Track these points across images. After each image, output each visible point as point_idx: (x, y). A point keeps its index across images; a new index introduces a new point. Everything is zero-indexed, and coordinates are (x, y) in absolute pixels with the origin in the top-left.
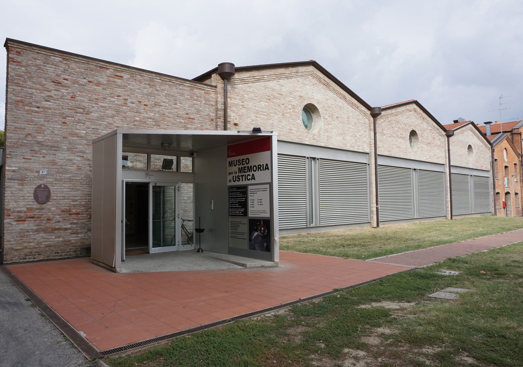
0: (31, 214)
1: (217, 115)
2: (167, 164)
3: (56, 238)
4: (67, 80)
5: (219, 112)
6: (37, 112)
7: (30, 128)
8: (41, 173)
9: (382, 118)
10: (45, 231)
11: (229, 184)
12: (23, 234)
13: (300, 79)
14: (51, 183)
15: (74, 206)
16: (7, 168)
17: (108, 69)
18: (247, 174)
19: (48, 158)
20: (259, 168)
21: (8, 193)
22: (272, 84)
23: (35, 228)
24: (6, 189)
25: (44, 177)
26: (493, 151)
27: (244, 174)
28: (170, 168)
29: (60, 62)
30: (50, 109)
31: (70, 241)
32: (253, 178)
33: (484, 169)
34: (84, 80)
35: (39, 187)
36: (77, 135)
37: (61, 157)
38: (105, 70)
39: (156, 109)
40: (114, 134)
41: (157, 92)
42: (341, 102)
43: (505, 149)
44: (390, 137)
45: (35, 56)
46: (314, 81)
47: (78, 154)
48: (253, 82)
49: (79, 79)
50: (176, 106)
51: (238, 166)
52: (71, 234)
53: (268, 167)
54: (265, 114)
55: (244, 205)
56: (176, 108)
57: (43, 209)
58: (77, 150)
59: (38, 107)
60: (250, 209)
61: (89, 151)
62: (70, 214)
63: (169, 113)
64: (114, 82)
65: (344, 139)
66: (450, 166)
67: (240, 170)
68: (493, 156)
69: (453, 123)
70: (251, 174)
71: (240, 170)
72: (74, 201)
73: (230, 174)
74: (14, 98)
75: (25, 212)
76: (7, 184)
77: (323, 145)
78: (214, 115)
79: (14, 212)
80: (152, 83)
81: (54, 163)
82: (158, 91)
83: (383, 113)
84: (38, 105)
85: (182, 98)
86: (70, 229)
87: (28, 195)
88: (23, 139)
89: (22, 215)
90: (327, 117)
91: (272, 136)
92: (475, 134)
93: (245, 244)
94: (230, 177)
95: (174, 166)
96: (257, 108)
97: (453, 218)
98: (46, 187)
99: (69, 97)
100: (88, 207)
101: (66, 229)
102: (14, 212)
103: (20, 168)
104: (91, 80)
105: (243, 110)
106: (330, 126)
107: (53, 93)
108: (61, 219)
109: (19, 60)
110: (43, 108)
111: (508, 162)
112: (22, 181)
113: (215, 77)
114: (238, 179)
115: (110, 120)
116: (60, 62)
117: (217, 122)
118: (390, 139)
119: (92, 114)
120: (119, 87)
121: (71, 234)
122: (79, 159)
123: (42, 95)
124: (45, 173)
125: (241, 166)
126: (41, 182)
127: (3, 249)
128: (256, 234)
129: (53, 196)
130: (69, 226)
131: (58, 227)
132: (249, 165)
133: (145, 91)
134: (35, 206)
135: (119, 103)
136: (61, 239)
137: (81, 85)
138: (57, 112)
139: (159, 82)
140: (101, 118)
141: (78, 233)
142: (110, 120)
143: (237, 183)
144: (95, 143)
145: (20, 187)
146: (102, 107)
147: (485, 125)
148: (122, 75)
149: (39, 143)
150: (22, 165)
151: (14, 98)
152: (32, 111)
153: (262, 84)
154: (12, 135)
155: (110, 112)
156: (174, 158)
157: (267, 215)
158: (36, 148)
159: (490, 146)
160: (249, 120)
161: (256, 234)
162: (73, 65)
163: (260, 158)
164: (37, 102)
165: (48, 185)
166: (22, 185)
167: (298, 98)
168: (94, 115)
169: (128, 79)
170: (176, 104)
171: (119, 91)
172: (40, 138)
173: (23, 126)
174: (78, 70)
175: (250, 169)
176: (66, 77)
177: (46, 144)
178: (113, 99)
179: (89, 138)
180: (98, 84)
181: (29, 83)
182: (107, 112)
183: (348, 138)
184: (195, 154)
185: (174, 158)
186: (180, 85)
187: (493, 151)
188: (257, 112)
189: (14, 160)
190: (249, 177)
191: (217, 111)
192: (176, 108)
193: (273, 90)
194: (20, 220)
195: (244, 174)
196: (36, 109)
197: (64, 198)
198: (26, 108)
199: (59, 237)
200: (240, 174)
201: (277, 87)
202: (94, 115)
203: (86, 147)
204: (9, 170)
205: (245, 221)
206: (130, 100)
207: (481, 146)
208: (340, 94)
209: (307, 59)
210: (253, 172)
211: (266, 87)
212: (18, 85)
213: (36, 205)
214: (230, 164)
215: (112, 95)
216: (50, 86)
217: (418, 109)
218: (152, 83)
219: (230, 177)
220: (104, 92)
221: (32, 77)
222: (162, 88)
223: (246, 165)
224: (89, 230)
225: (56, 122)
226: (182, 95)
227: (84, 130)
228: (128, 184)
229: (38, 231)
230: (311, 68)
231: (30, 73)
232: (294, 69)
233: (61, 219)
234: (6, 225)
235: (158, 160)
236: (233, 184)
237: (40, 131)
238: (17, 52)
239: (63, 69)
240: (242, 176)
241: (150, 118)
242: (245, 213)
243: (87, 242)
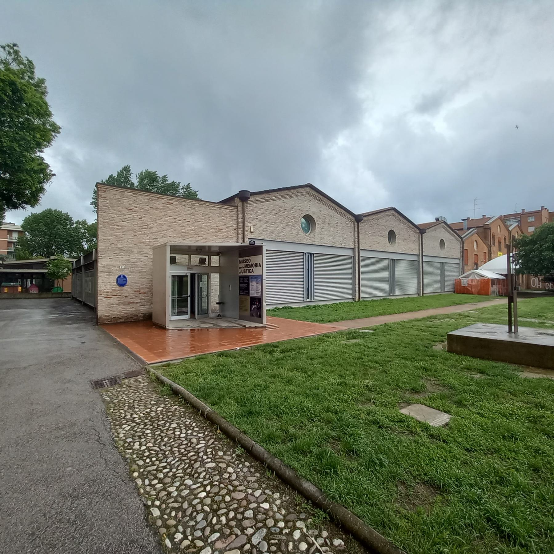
0: (114, 293)
1: (238, 226)
2: (202, 261)
3: (130, 308)
4: (136, 207)
5: (239, 224)
6: (117, 229)
7: (113, 239)
8: (121, 268)
9: (365, 222)
10: (124, 304)
11: (240, 275)
12: (110, 305)
13: (300, 198)
14: (127, 274)
15: (142, 288)
16: (99, 265)
17: (163, 199)
18: (249, 269)
19: (125, 258)
20: (256, 265)
21: (100, 281)
22: (278, 202)
23: (118, 302)
24: (99, 278)
25: (123, 270)
26: (463, 243)
27: (247, 269)
28: (204, 264)
29: (132, 196)
30: (126, 227)
31: (140, 310)
32: (253, 272)
33: (455, 257)
34: (147, 207)
35: (120, 276)
36: (143, 243)
37: (133, 257)
38: (161, 200)
39: (195, 224)
40: (165, 245)
41: (196, 212)
42: (332, 212)
43: (476, 241)
44: (371, 236)
45: (115, 192)
46: (311, 198)
47: (145, 255)
48: (264, 202)
49: (144, 206)
50: (209, 221)
51: (244, 264)
52: (140, 305)
53: (259, 265)
54: (273, 223)
55: (247, 289)
56: (209, 223)
57: (122, 290)
58: (144, 252)
59: (118, 226)
60: (251, 292)
61: (151, 252)
62: (140, 293)
63: (204, 226)
64: (167, 207)
65: (333, 239)
66: (422, 256)
67: (246, 266)
68: (463, 247)
69: (435, 221)
70: (251, 268)
71: (246, 266)
72: (142, 285)
73: (240, 268)
74: (102, 220)
75: (111, 292)
76: (99, 275)
77: (317, 244)
78: (236, 226)
79: (104, 292)
80: (193, 207)
81: (128, 261)
82: (197, 211)
83: (364, 218)
84: (118, 224)
85: (213, 215)
86: (140, 303)
87: (113, 281)
88: (109, 246)
89: (109, 294)
90: (320, 223)
91: (262, 246)
92: (447, 230)
93: (248, 313)
94: (240, 270)
95: (207, 263)
96: (267, 220)
97: (424, 295)
98: (124, 276)
99: (138, 218)
100: (150, 289)
101: (137, 303)
102: (104, 292)
103: (107, 265)
104: (152, 206)
105: (257, 222)
106: (323, 230)
107: (127, 216)
108: (134, 297)
109: (105, 196)
110: (121, 226)
111: (478, 252)
112: (109, 273)
113: (237, 200)
114: (244, 271)
115: (165, 232)
116: (132, 196)
117: (238, 231)
118: (371, 238)
119: (153, 229)
120: (171, 210)
121: (140, 305)
122: (145, 258)
123: (120, 218)
124: (123, 268)
125: (246, 263)
126: (121, 274)
127: (98, 316)
128: (254, 306)
129: (129, 281)
130: (139, 301)
131: (132, 301)
132: (250, 263)
133: (188, 212)
134: (117, 289)
135: (171, 221)
136: (134, 309)
137: (145, 210)
138: (131, 228)
139: (198, 206)
140: (159, 232)
141: (145, 305)
142: (165, 232)
143: (244, 274)
144: (154, 249)
145: (108, 277)
146: (159, 224)
147: (462, 221)
148: (172, 202)
149: (119, 248)
150: (108, 263)
151: (102, 220)
152: (114, 228)
153: (271, 202)
154: (102, 244)
155: (165, 227)
156: (207, 257)
157: (259, 296)
158: (117, 252)
159: (460, 240)
160: (262, 228)
161: (254, 306)
162: (140, 197)
163: (254, 260)
164: (117, 223)
165: (125, 275)
166: (109, 275)
167: (298, 211)
168: (155, 229)
169: (176, 205)
170: (209, 220)
171: (170, 213)
172: (119, 245)
173: (109, 238)
174: (143, 200)
175: (251, 266)
176: (136, 206)
177: (124, 249)
178: (166, 219)
179: (151, 244)
180: (157, 209)
181: (112, 210)
182: (163, 227)
183: (337, 238)
184: (220, 255)
185: (207, 257)
186: (212, 207)
187: (463, 243)
188: (267, 222)
189: (103, 260)
190: (250, 271)
191: (238, 223)
192: (209, 223)
193: (280, 206)
194: (108, 297)
195: (247, 269)
196: (117, 227)
197: (136, 283)
198: (111, 226)
199: (133, 308)
200: (246, 269)
201: (283, 204)
202: (155, 229)
203: (150, 250)
204: (101, 266)
205: (249, 298)
206: (178, 219)
207: (453, 239)
208: (331, 206)
209: (306, 183)
210: (253, 268)
211: (274, 205)
212: (105, 212)
213: (118, 288)
214: (241, 262)
215: (166, 216)
216: (126, 212)
217: (396, 214)
218: (193, 207)
219: (240, 270)
220: (161, 214)
221: (114, 207)
222: (200, 209)
223: (249, 263)
224: (152, 304)
225: (130, 235)
226: (214, 213)
227: (148, 239)
228: (173, 276)
229: (119, 304)
230: (308, 189)
231: (112, 204)
232: (295, 191)
233: (134, 297)
234: (99, 301)
235: (195, 259)
236: (241, 274)
237: (120, 240)
238: (103, 191)
239: (133, 200)
240: (247, 270)
241: (192, 230)
242: (249, 295)
243: (150, 311)
